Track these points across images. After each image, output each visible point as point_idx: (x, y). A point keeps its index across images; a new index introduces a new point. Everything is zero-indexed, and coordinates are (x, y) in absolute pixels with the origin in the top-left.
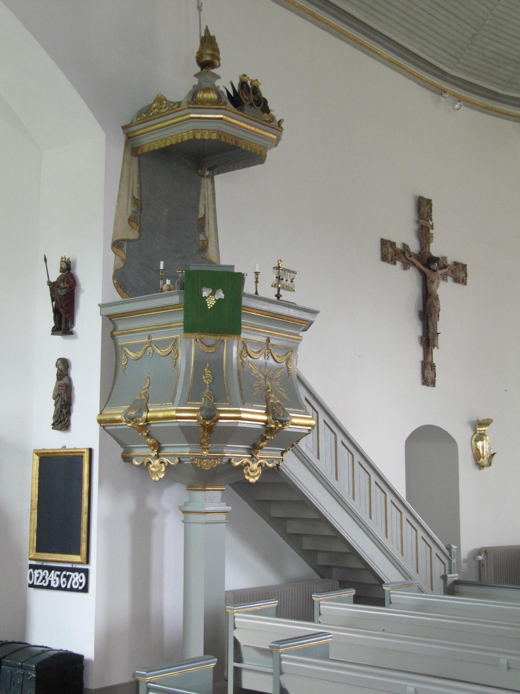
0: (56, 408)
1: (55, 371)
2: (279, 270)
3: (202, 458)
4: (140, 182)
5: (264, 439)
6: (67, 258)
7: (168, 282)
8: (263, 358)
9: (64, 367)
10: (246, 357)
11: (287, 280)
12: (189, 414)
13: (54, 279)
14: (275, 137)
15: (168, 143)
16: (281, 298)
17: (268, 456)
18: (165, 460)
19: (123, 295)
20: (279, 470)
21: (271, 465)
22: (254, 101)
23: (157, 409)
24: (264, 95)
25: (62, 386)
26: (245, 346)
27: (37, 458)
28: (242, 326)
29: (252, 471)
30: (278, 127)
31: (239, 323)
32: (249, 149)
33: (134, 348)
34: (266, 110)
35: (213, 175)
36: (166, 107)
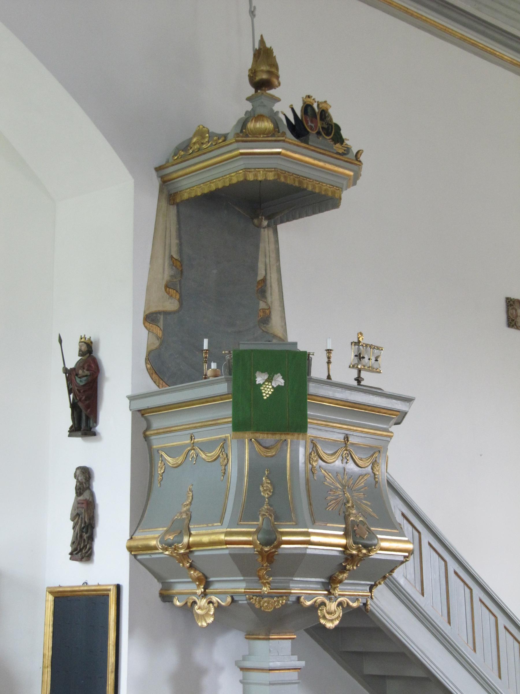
0: (74, 532)
1: (73, 483)
2: (359, 345)
3: (261, 596)
4: (180, 237)
5: (343, 570)
6: (87, 337)
7: (214, 366)
8: (340, 462)
9: (85, 478)
10: (316, 461)
11: (369, 359)
12: (245, 537)
13: (71, 364)
14: (352, 173)
15: (213, 187)
16: (362, 383)
17: (351, 592)
18: (214, 599)
19: (159, 383)
20: (367, 610)
21: (355, 605)
22: (323, 128)
23: (201, 532)
24: (335, 120)
25: (83, 503)
26: (315, 446)
27: (51, 598)
28: (309, 420)
29: (329, 613)
30: (355, 161)
31: (304, 416)
32: (317, 190)
33: (172, 451)
34: (338, 139)
35: (276, 224)
36: (208, 142)
